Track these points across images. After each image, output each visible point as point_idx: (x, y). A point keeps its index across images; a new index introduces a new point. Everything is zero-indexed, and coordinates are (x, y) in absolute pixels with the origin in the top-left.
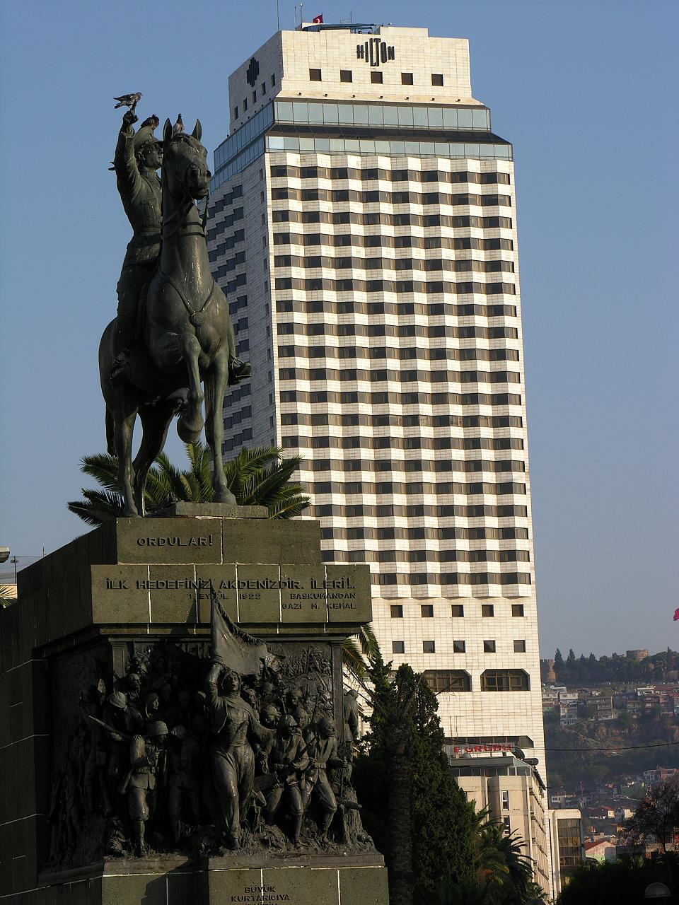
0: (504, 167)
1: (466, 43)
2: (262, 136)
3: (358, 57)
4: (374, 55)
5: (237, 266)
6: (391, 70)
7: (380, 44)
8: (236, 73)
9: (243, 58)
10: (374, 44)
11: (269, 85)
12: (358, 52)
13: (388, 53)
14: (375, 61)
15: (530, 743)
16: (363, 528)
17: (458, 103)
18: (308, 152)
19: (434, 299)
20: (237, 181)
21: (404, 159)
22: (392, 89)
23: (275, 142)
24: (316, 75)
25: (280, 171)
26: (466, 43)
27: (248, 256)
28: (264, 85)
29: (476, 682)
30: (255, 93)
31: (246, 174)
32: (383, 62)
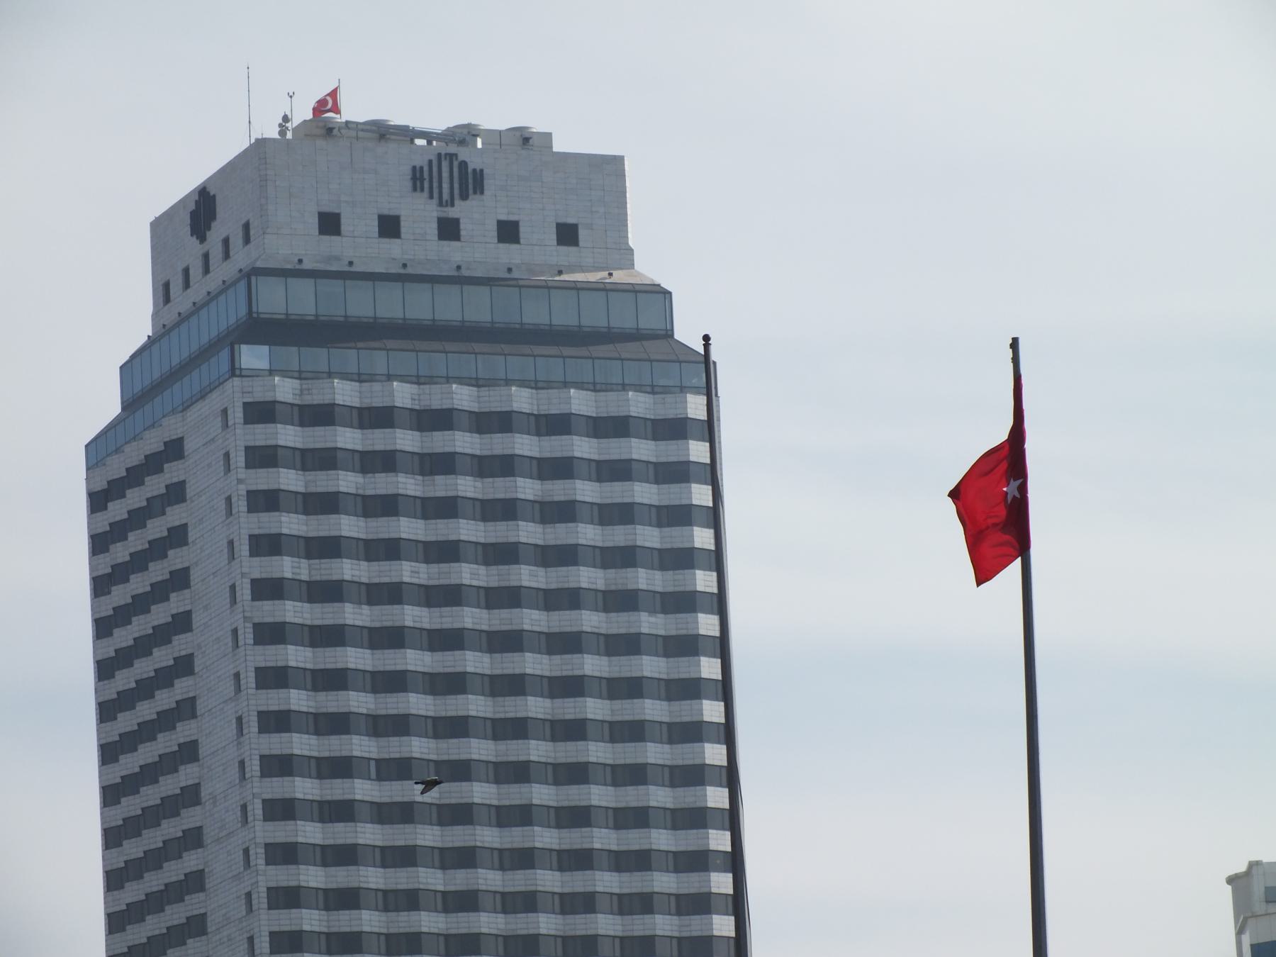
1: (555, 149)
3: (415, 189)
4: (446, 186)
5: (173, 596)
6: (470, 213)
7: (456, 164)
10: (445, 165)
12: (414, 179)
14: (446, 196)
16: (650, 850)
17: (402, 271)
19: (564, 667)
20: (172, 428)
21: (503, 390)
26: (555, 149)
27: (195, 576)
28: (226, 242)
30: (206, 257)
31: (193, 414)
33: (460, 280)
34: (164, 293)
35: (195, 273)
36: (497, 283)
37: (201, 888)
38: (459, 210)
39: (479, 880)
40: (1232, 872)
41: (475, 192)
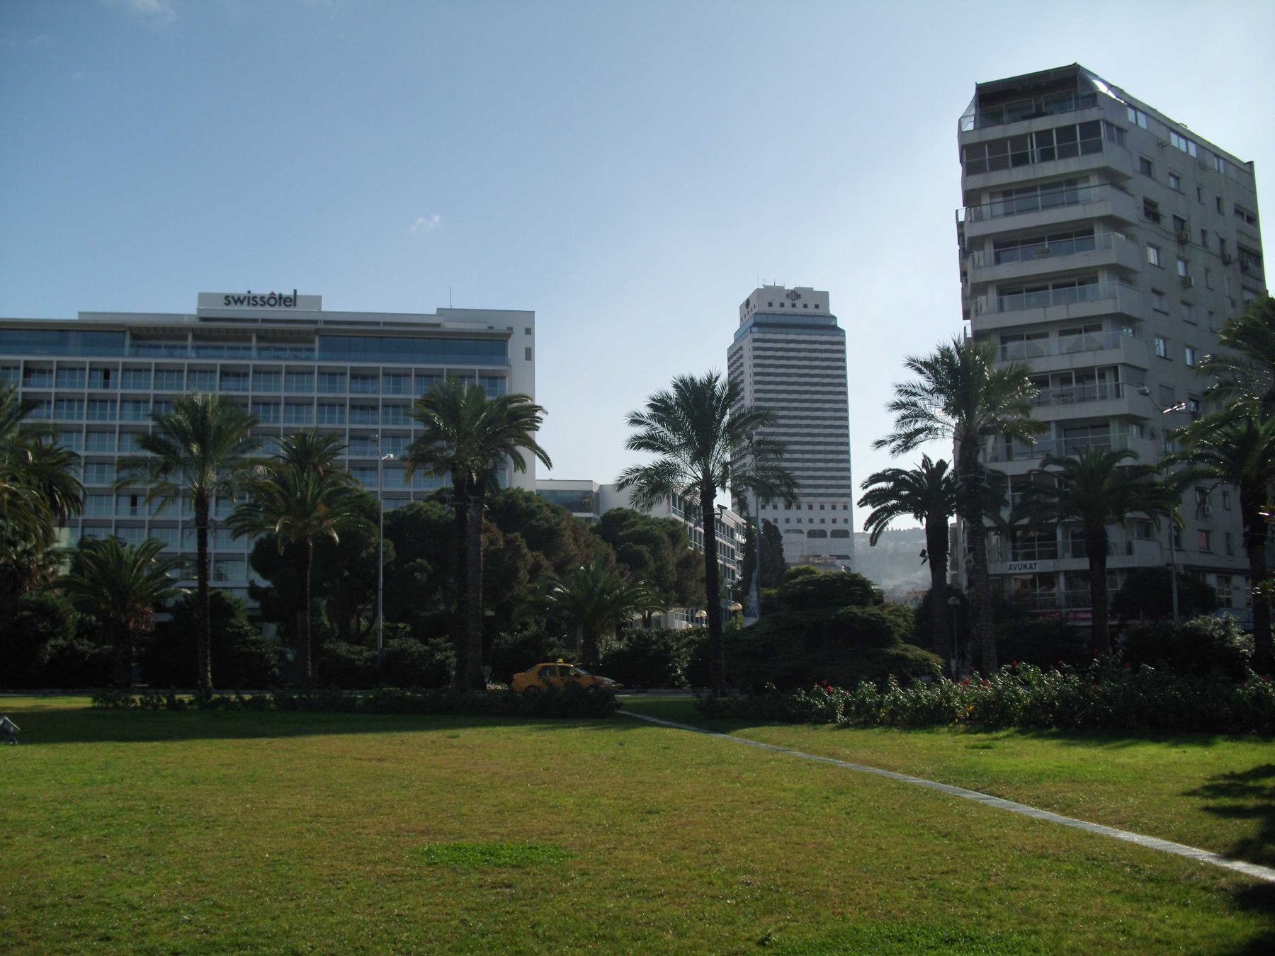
6: (799, 303)
20: (740, 344)
22: (799, 309)
33: (795, 315)
34: (742, 319)
36: (147, 343)
38: (796, 302)
39: (989, 202)
40: (914, 356)
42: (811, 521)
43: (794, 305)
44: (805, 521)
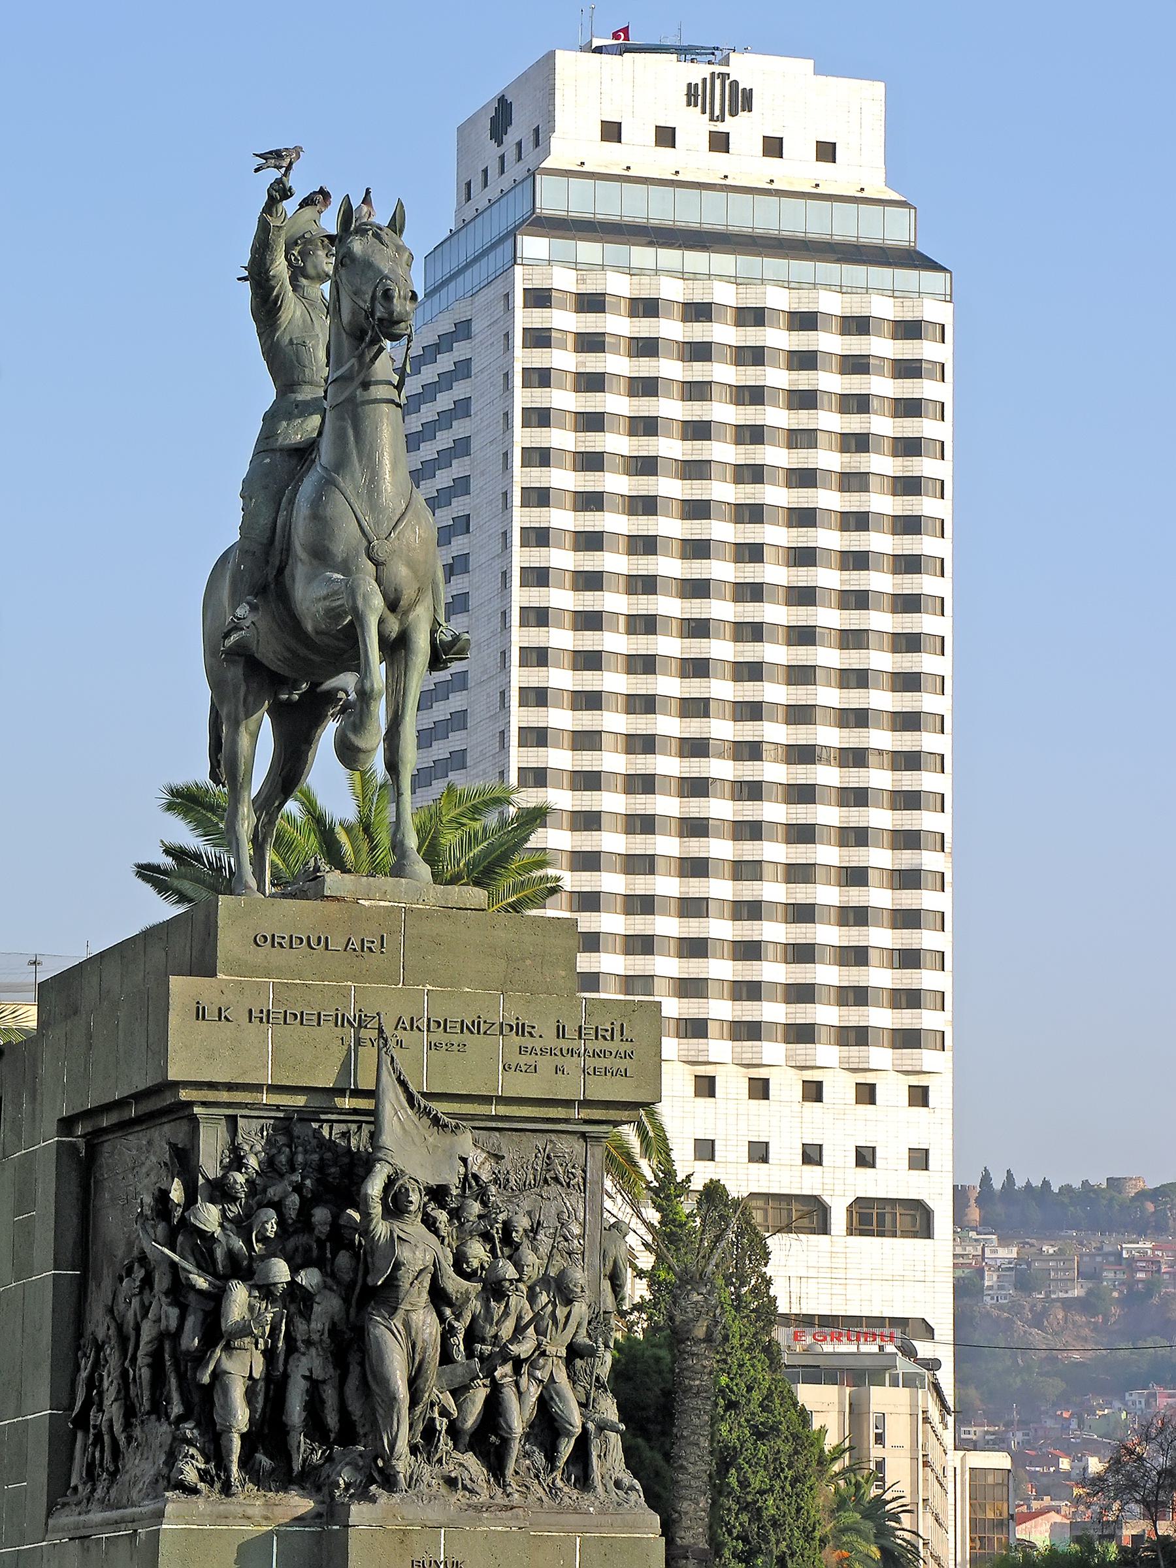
0: (936, 311)
2: (511, 235)
3: (689, 104)
8: (471, 121)
9: (485, 96)
10: (718, 82)
11: (528, 146)
13: (741, 100)
14: (717, 112)
15: (928, 1331)
18: (591, 267)
23: (533, 246)
24: (612, 132)
25: (539, 298)
28: (519, 144)
29: (839, 1219)
30: (502, 158)
32: (732, 115)
35: (493, 172)
37: (468, 337)
41: (743, 110)
42: (865, 1158)
43: (720, 143)
44: (839, 1155)
